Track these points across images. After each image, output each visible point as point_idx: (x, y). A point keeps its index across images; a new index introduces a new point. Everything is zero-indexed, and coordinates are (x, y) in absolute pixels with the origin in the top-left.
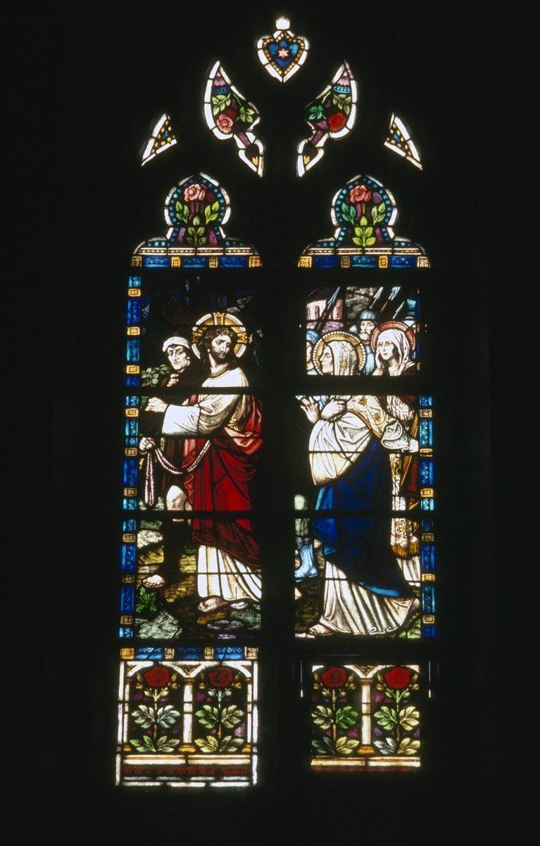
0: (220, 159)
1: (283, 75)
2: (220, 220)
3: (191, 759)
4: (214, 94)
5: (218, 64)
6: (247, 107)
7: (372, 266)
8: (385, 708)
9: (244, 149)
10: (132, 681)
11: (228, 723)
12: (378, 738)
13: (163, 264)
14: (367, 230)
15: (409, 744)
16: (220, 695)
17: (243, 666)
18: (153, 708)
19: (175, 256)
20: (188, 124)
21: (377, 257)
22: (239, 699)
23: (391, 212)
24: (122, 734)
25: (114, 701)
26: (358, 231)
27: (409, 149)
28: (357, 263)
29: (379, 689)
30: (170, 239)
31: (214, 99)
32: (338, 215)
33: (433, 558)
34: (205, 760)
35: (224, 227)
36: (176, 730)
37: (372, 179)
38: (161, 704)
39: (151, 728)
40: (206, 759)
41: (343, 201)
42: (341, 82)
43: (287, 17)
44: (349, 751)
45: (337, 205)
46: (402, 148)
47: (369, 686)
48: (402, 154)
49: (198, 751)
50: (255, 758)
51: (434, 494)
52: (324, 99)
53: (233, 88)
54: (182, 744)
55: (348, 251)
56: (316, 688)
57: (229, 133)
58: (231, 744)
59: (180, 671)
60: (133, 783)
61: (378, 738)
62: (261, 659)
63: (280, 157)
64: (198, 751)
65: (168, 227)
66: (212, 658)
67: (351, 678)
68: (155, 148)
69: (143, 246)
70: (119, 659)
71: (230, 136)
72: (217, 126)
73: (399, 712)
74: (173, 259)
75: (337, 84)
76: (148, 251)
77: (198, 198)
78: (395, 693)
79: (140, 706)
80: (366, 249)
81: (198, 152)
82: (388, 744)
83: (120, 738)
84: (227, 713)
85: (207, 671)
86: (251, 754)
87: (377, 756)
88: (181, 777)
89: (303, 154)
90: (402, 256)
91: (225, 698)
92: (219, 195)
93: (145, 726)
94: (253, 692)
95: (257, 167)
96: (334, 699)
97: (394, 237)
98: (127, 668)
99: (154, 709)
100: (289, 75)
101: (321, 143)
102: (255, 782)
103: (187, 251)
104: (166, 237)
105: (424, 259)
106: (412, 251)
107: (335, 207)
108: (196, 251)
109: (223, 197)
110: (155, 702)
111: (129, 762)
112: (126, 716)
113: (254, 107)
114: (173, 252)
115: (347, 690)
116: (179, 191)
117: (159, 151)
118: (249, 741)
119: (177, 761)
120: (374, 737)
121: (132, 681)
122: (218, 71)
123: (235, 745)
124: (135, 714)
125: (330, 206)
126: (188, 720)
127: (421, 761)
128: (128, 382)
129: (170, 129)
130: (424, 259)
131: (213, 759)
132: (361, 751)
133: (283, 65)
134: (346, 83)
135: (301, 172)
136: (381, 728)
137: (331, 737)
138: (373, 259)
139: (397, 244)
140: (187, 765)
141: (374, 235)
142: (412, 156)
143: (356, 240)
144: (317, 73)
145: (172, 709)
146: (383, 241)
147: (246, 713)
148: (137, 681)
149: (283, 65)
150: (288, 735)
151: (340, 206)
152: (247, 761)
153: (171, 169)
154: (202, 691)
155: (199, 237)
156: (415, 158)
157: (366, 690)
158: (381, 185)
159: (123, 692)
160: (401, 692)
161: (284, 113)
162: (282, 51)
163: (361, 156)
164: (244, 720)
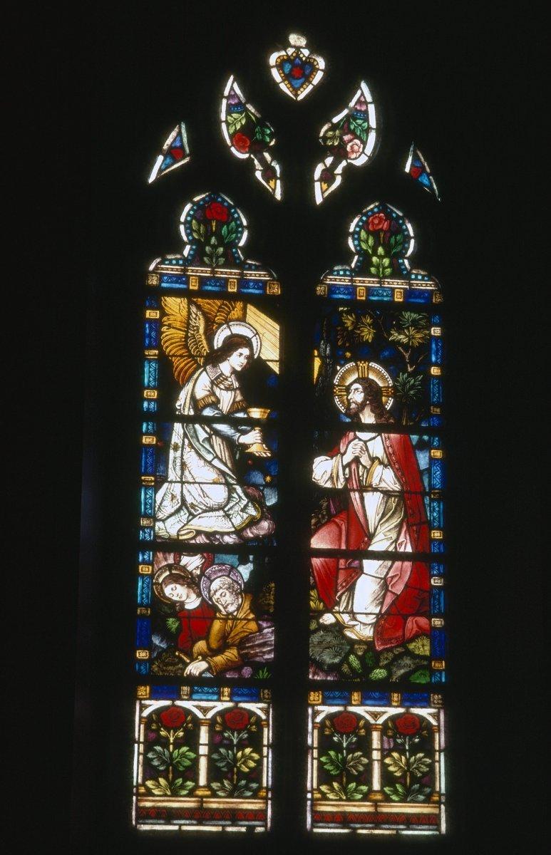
3: (206, 802)
4: (229, 113)
6: (263, 126)
8: (395, 755)
9: (261, 170)
14: (384, 260)
17: (260, 709)
18: (232, 751)
21: (393, 290)
22: (255, 742)
23: (242, 233)
25: (306, 749)
31: (229, 117)
34: (398, 808)
35: (241, 248)
39: (404, 776)
41: (361, 228)
45: (186, 222)
54: (370, 791)
55: (197, 271)
56: (327, 733)
58: (247, 788)
59: (368, 717)
63: (298, 182)
64: (214, 795)
65: (184, 244)
67: (189, 718)
73: (410, 759)
78: (342, 737)
79: (329, 752)
81: (211, 169)
82: (334, 788)
85: (393, 719)
86: (439, 803)
87: (213, 798)
88: (339, 823)
89: (321, 180)
91: (241, 740)
92: (236, 216)
93: (398, 774)
100: (302, 95)
101: (339, 170)
103: (205, 272)
104: (182, 254)
108: (213, 272)
109: (239, 218)
111: (142, 804)
115: (249, 732)
116: (364, 218)
118: (265, 785)
119: (366, 808)
121: (148, 722)
122: (232, 88)
123: (361, 792)
124: (150, 755)
126: (203, 763)
128: (145, 404)
130: (324, 291)
132: (199, 793)
135: (319, 200)
136: (155, 767)
139: (247, 266)
141: (391, 265)
146: (397, 272)
151: (190, 222)
152: (435, 811)
153: (176, 187)
154: (153, 731)
155: (384, 268)
158: (401, 214)
160: (239, 734)
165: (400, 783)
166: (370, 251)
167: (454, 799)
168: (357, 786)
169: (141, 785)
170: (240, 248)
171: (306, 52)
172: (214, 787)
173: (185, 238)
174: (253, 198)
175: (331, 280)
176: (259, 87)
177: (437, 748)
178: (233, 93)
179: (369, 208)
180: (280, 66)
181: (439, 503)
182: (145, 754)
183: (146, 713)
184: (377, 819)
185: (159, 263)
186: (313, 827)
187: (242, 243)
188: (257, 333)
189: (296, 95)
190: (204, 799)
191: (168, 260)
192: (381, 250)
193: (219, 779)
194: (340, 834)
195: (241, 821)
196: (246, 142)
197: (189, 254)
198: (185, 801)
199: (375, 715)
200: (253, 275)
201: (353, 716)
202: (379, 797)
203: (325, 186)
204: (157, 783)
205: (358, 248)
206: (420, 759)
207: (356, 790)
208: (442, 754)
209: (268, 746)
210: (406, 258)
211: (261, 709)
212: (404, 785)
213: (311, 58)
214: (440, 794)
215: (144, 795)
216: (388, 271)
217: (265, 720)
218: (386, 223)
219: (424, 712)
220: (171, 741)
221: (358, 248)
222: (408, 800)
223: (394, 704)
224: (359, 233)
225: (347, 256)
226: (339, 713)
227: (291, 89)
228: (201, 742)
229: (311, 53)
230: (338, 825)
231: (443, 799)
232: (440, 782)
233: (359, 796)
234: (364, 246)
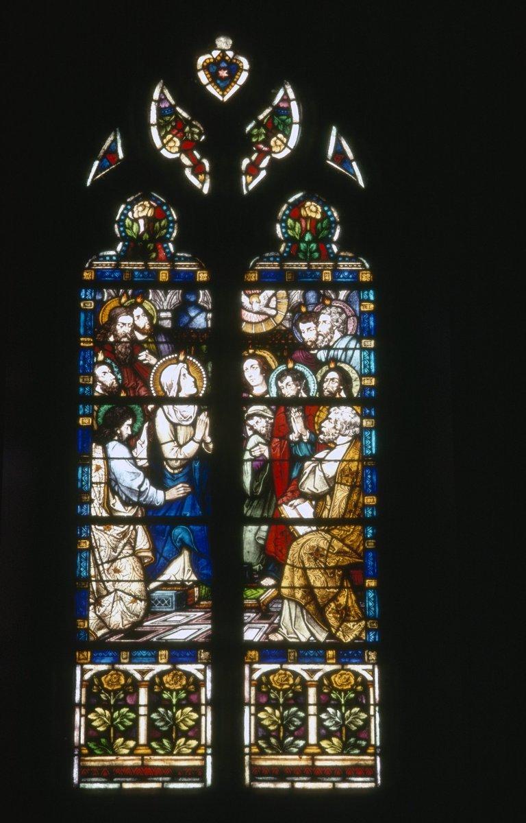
1: (223, 96)
14: (312, 245)
17: (304, 670)
18: (172, 710)
19: (164, 270)
21: (157, 272)
24: (79, 736)
25: (72, 706)
29: (264, 690)
30: (120, 252)
32: (284, 230)
34: (157, 762)
36: (132, 733)
40: (331, 760)
44: (126, 751)
47: (147, 689)
49: (323, 752)
50: (209, 759)
53: (178, 109)
54: (307, 745)
57: (176, 153)
58: (356, 746)
60: (97, 785)
62: (378, 662)
63: (226, 175)
64: (154, 753)
66: (334, 661)
69: (258, 261)
71: (178, 155)
77: (147, 214)
83: (76, 739)
84: (351, 714)
88: (138, 778)
90: (136, 270)
91: (179, 701)
92: (168, 213)
94: (375, 694)
96: (281, 700)
97: (338, 252)
98: (83, 672)
99: (172, 712)
100: (226, 99)
102: (379, 782)
105: (91, 276)
112: (253, 718)
113: (199, 125)
119: (304, 762)
120: (320, 737)
123: (359, 747)
124: (154, 716)
126: (143, 723)
132: (308, 751)
133: (224, 85)
136: (327, 728)
137: (108, 738)
141: (318, 250)
145: (191, 711)
147: (200, 715)
149: (224, 85)
157: (312, 692)
159: (79, 695)
161: (224, 134)
162: (225, 70)
163: (305, 171)
165: (274, 737)
167: (385, 751)
168: (124, 741)
169: (253, 745)
171: (230, 54)
174: (179, 193)
175: (288, 266)
176: (190, 93)
177: (203, 701)
178: (285, 97)
180: (206, 67)
181: (372, 471)
182: (256, 715)
183: (256, 676)
184: (143, 773)
185: (258, 261)
186: (80, 781)
187: (336, 238)
190: (145, 757)
191: (266, 257)
192: (308, 237)
194: (194, 789)
195: (352, 776)
199: (143, 673)
200: (343, 266)
202: (315, 750)
204: (190, 747)
206: (356, 714)
207: (124, 745)
208: (209, 709)
209: (375, 705)
210: (171, 242)
211: (199, 670)
212: (277, 738)
215: (86, 755)
218: (150, 211)
219: (191, 668)
220: (343, 702)
221: (286, 236)
222: (175, 753)
224: (285, 221)
227: (218, 90)
229: (236, 54)
230: (103, 780)
231: (209, 751)
232: (375, 733)
233: (295, 750)
234: (290, 232)
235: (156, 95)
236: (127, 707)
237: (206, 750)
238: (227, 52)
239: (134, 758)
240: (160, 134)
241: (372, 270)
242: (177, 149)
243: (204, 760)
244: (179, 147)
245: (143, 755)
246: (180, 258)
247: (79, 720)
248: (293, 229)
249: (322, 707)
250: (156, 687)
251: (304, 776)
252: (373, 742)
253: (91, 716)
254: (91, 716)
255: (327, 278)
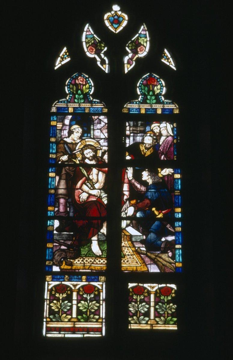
0: (90, 67)
2: (89, 92)
5: (87, 25)
7: (82, 112)
10: (51, 291)
11: (142, 310)
12: (152, 316)
13: (154, 112)
15: (65, 317)
16: (138, 298)
17: (72, 284)
20: (76, 51)
21: (156, 109)
22: (97, 298)
24: (46, 313)
25: (43, 300)
26: (77, 96)
27: (170, 62)
28: (132, 111)
32: (140, 90)
33: (180, 238)
35: (163, 96)
36: (147, 314)
37: (155, 75)
38: (91, 300)
42: (142, 33)
43: (119, 5)
46: (168, 61)
48: (168, 64)
51: (181, 210)
52: (135, 40)
56: (130, 295)
59: (71, 286)
61: (152, 316)
62: (107, 282)
67: (68, 289)
68: (61, 61)
69: (57, 103)
70: (45, 280)
72: (88, 51)
74: (70, 108)
75: (141, 34)
76: (129, 106)
80: (80, 104)
81: (81, 64)
84: (64, 304)
93: (57, 310)
94: (103, 295)
95: (105, 69)
97: (93, 100)
98: (48, 285)
100: (118, 31)
106: (172, 106)
107: (139, 87)
108: (79, 105)
110: (60, 300)
111: (48, 325)
114: (170, 106)
117: (63, 63)
119: (69, 325)
121: (51, 291)
122: (88, 28)
124: (157, 307)
125: (137, 87)
126: (152, 309)
127: (178, 327)
129: (68, 54)
131: (91, 324)
132: (72, 320)
134: (145, 33)
135: (126, 71)
136: (158, 312)
138: (155, 110)
140: (74, 327)
142: (172, 65)
143: (76, 100)
144: (132, 29)
146: (158, 102)
147: (100, 305)
148: (53, 290)
150: (118, 313)
152: (100, 326)
153: (66, 70)
156: (173, 66)
157: (152, 296)
159: (47, 295)
161: (116, 45)
162: (116, 18)
163: (150, 65)
164: (99, 307)
166: (147, 93)
170: (91, 95)
172: (51, 317)
173: (67, 92)
176: (100, 28)
179: (74, 75)
180: (108, 19)
182: (49, 304)
185: (57, 103)
186: (46, 333)
188: (74, 129)
189: (116, 31)
193: (159, 317)
196: (93, 49)
197: (141, 100)
198: (84, 324)
199: (75, 286)
201: (169, 288)
202: (75, 320)
203: (129, 66)
205: (141, 93)
207: (143, 320)
209: (103, 300)
213: (122, 15)
214: (102, 319)
216: (154, 101)
217: (101, 290)
221: (141, 93)
223: (84, 281)
224: (69, 85)
225: (65, 95)
226: (136, 286)
228: (73, 299)
231: (104, 321)
233: (95, 320)
235: (86, 29)
236: (95, 301)
237: (102, 320)
238: (118, 12)
239: (98, 323)
240: (86, 46)
241: (180, 109)
242: (94, 53)
243: (102, 324)
244: (95, 52)
245: (74, 322)
246: (95, 102)
247: (46, 308)
248: (73, 89)
249: (79, 302)
250: (53, 292)
251: (57, 331)
252: (101, 316)
253: (52, 305)
254: (52, 305)
255: (143, 111)
